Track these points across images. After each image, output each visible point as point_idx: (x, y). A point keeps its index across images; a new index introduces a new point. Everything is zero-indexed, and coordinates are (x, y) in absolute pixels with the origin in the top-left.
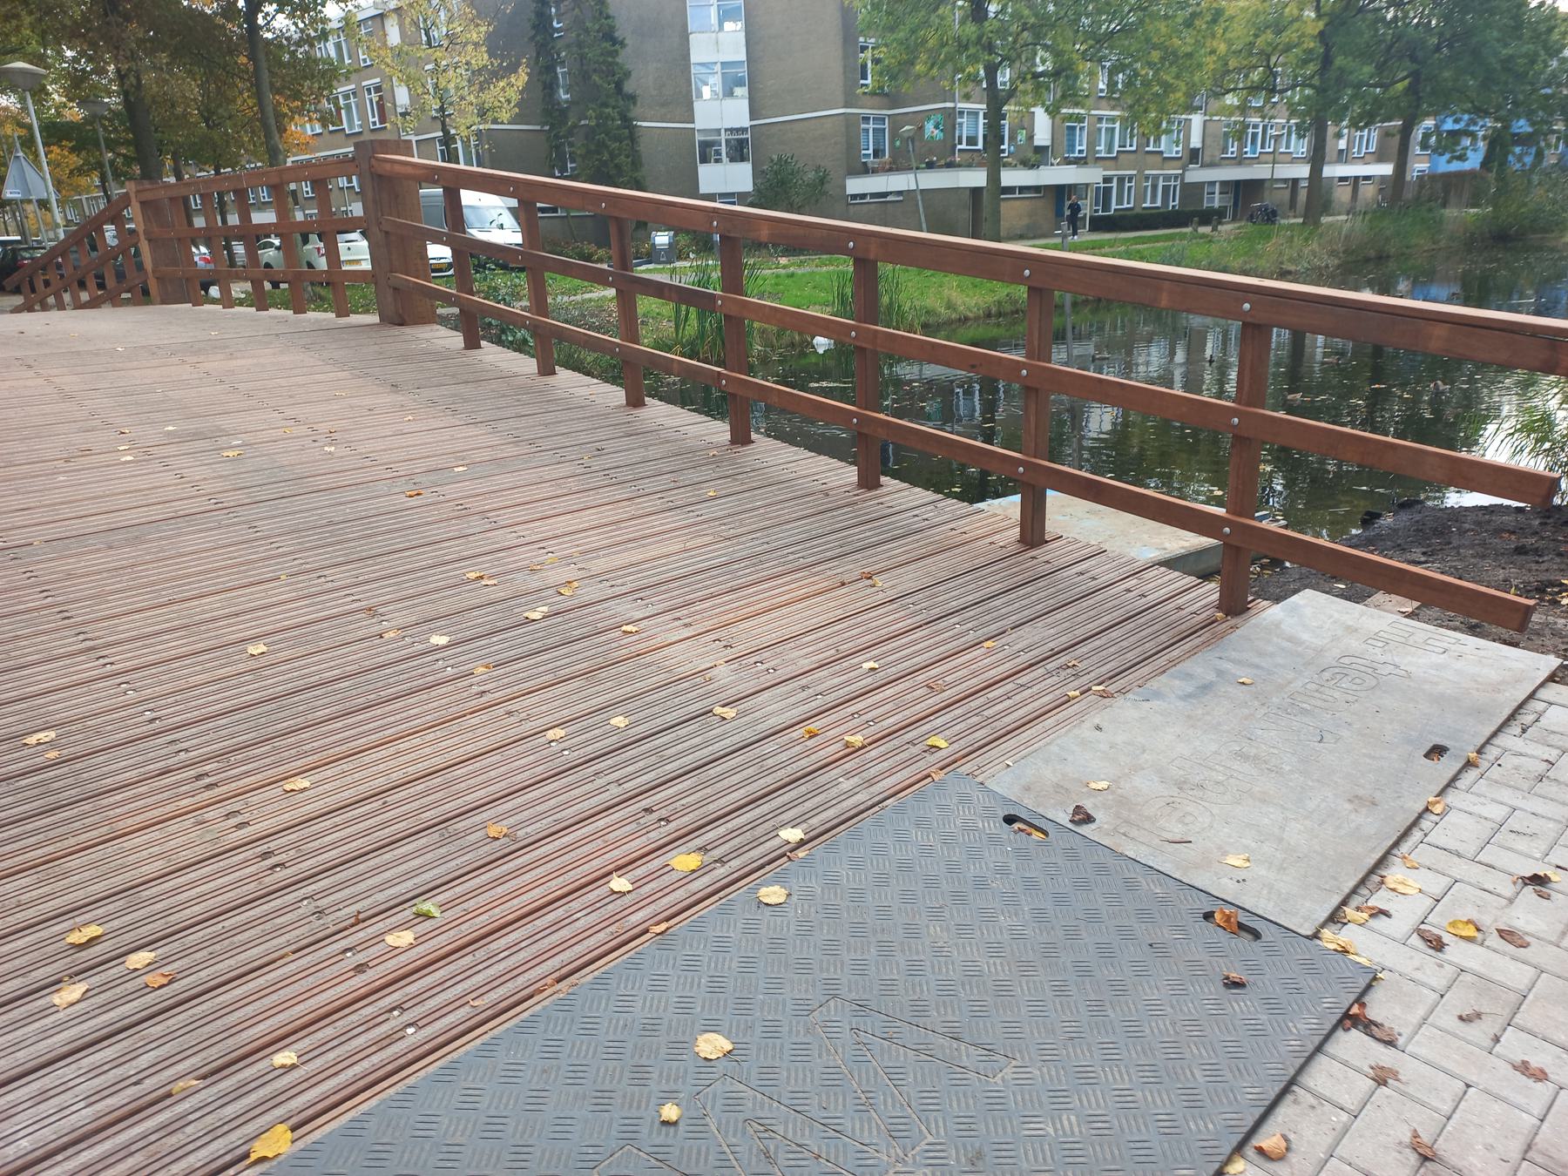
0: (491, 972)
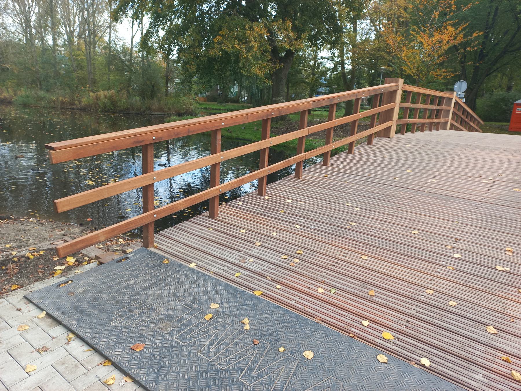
0: (320, 309)
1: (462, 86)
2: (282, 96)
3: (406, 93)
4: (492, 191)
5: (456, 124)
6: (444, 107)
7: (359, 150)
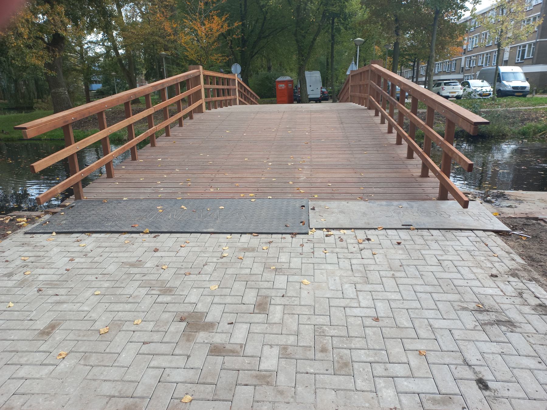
1: (237, 68)
2: (62, 86)
3: (206, 77)
4: (278, 134)
5: (242, 100)
6: (231, 87)
7: (175, 131)
